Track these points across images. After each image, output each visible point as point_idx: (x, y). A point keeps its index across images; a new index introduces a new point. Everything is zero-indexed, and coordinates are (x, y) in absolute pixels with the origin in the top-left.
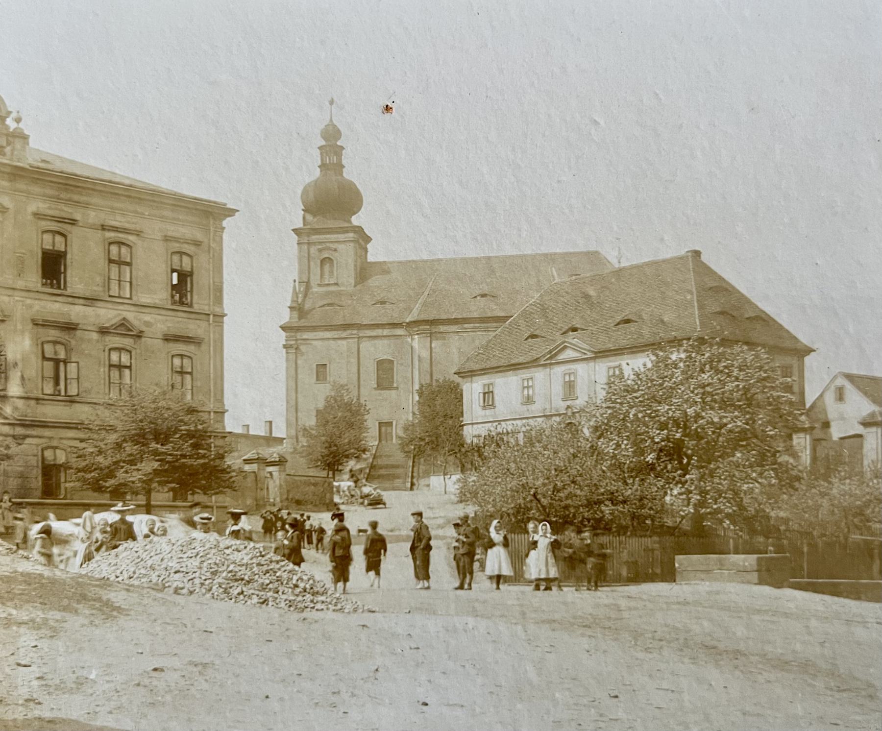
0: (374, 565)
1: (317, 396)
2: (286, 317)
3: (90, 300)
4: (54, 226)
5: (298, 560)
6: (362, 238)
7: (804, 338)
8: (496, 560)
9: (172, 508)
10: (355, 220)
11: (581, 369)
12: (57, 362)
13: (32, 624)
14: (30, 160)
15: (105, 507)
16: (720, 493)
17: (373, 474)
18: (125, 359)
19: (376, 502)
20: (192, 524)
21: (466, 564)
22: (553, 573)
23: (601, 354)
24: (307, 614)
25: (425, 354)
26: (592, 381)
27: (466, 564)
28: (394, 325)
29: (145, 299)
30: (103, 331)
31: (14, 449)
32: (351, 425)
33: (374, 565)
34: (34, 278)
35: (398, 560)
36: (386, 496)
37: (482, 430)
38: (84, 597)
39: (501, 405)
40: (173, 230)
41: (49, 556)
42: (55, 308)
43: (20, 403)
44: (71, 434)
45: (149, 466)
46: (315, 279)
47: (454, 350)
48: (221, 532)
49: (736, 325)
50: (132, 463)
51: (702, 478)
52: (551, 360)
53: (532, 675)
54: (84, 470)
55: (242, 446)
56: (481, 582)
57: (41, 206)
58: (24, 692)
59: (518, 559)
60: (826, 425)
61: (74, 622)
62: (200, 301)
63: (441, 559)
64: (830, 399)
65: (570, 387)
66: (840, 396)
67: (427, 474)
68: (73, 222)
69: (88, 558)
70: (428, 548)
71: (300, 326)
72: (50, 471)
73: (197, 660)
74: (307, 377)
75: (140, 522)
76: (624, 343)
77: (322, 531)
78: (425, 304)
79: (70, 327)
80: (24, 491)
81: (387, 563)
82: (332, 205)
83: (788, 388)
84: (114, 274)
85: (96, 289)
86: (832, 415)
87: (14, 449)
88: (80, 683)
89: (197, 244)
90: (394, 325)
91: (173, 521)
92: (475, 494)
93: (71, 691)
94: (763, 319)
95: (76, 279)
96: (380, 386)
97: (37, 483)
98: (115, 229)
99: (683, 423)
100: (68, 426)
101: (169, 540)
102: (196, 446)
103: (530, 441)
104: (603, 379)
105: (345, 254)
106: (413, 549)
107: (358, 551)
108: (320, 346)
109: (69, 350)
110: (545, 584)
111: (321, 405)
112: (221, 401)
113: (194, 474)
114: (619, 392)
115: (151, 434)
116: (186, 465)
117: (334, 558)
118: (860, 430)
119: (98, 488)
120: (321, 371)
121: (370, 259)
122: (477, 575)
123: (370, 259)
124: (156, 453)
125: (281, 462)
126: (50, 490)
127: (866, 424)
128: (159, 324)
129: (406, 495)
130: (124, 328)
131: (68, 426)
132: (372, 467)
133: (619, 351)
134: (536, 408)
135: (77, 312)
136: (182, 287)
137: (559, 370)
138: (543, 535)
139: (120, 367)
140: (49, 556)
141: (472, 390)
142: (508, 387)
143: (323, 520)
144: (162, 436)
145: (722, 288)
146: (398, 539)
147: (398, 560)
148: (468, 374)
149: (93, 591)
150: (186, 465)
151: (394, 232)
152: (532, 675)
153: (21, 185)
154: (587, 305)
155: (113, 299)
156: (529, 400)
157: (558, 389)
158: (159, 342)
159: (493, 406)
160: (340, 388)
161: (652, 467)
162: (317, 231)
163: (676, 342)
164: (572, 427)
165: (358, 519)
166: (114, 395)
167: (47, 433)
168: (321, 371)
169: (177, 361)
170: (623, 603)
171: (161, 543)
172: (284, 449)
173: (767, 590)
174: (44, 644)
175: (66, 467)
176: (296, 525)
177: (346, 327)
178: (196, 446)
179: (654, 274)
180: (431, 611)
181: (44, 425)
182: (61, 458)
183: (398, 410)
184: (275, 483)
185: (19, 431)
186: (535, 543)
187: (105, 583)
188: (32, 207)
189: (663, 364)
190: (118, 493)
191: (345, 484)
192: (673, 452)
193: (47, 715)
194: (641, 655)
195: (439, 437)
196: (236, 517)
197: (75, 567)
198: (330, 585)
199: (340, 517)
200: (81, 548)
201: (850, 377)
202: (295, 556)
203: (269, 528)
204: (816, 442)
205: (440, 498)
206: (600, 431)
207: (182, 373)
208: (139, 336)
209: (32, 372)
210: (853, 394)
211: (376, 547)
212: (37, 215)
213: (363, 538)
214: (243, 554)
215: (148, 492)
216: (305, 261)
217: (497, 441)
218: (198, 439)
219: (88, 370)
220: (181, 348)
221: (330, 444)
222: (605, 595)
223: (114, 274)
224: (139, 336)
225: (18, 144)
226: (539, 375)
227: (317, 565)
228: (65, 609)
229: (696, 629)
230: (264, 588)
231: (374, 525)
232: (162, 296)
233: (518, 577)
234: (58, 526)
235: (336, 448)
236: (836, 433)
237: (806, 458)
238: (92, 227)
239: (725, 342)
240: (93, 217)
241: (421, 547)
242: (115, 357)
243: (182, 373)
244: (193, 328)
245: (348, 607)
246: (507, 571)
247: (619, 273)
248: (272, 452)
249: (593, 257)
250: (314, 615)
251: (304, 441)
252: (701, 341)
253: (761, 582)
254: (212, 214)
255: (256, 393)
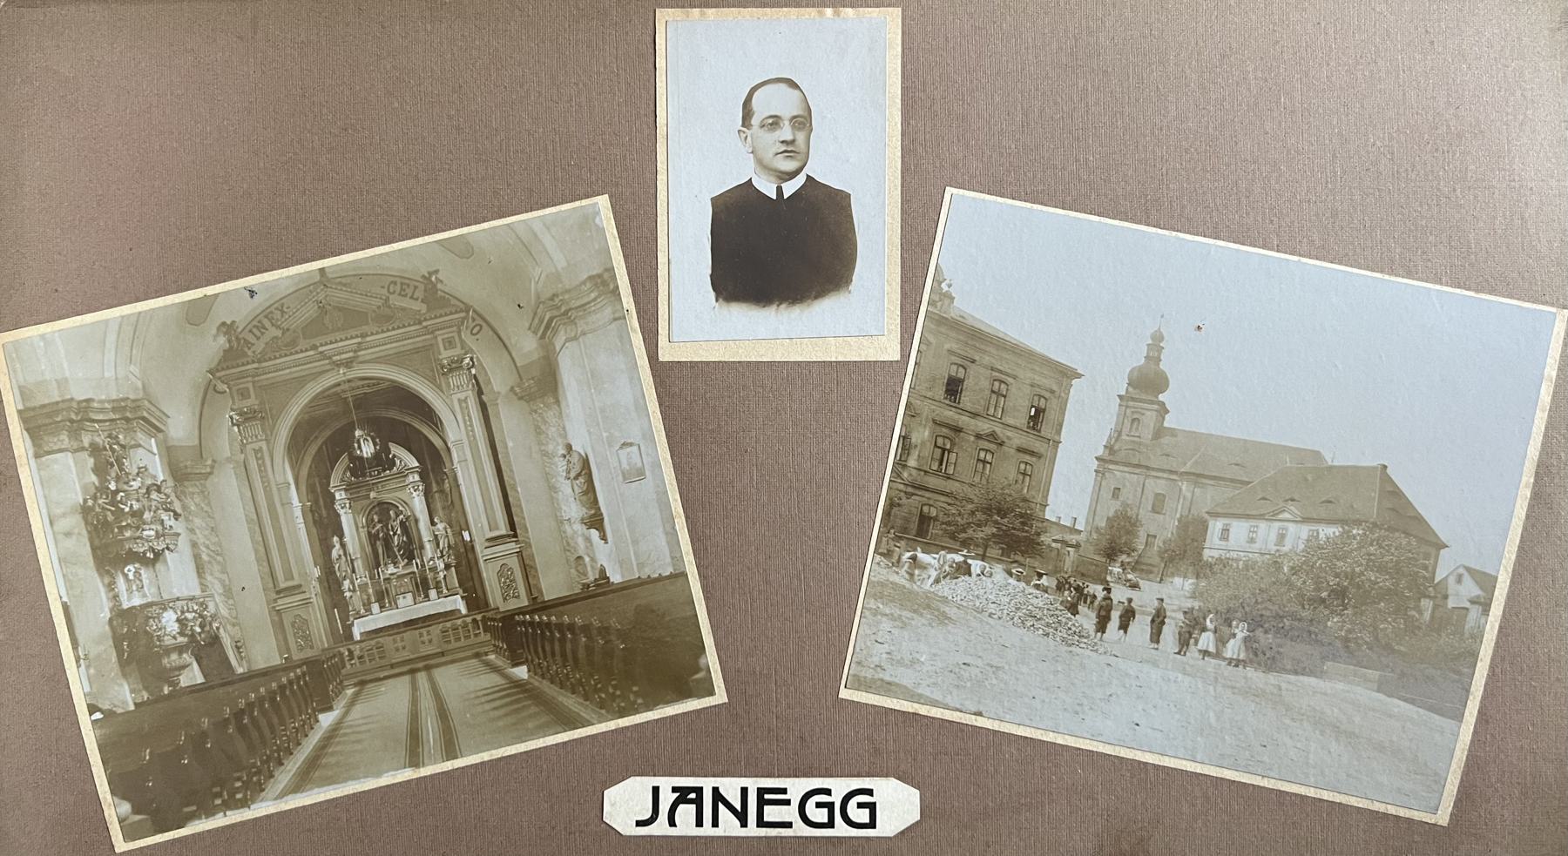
0: (1124, 627)
1: (1110, 508)
2: (1100, 451)
3: (975, 415)
4: (959, 361)
5: (1075, 612)
6: (1163, 410)
7: (1443, 537)
8: (1207, 640)
9: (999, 561)
10: (1161, 397)
11: (1292, 527)
12: (944, 450)
13: (892, 617)
14: (953, 314)
15: (956, 551)
16: (1364, 626)
17: (1136, 567)
18: (989, 458)
19: (1135, 586)
20: (1011, 574)
21: (1185, 640)
22: (1242, 657)
23: (1306, 520)
24: (1073, 648)
25: (1189, 495)
26: (1297, 535)
27: (1185, 640)
28: (1171, 472)
29: (1011, 421)
30: (978, 436)
31: (904, 501)
32: (1128, 532)
33: (1124, 627)
34: (940, 392)
35: (1141, 627)
36: (1141, 583)
37: (1216, 554)
38: (928, 606)
39: (1236, 540)
40: (1038, 379)
41: (912, 575)
42: (950, 414)
43: (914, 472)
44: (943, 498)
45: (990, 530)
46: (1125, 431)
47: (1207, 497)
48: (1028, 583)
49: (1399, 515)
50: (979, 526)
51: (1355, 614)
52: (1272, 517)
53: (1213, 720)
54: (948, 523)
55: (1054, 530)
56: (1193, 652)
57: (954, 346)
58: (876, 660)
59: (1222, 641)
60: (1446, 597)
61: (918, 621)
62: (1046, 430)
63: (1169, 633)
64: (1452, 580)
65: (1281, 537)
66: (1459, 580)
67: (1173, 575)
68: (973, 361)
69: (937, 581)
70: (1163, 623)
71: (1109, 459)
72: (924, 520)
73: (994, 663)
74: (1106, 494)
75: (976, 566)
76: (1324, 516)
77: (1095, 597)
78: (1196, 462)
79: (958, 430)
80: (905, 530)
81: (1133, 627)
82: (1147, 384)
83: (1425, 568)
84: (993, 402)
85: (980, 409)
86: (1450, 592)
87: (904, 501)
88: (914, 662)
89: (1052, 392)
90: (1171, 472)
91: (998, 569)
92: (1201, 594)
93: (906, 666)
94: (1419, 519)
95: (966, 400)
96: (1154, 511)
97: (914, 526)
98: (1000, 372)
99: (1351, 576)
100: (942, 493)
101: (994, 582)
102: (1023, 524)
103: (1247, 567)
104: (1304, 535)
105: (1149, 418)
106: (1153, 621)
107: (1115, 615)
108: (1119, 474)
109: (953, 444)
110: (1237, 663)
111: (1111, 514)
112: (1046, 497)
113: (1018, 541)
114: (1313, 545)
115: (995, 509)
116: (1014, 534)
117: (1098, 616)
118: (1468, 605)
119: (953, 537)
120: (1116, 492)
121: (1166, 424)
122: (1192, 647)
123: (1166, 424)
124: (996, 522)
125: (1077, 546)
126: (922, 531)
127: (1472, 602)
128: (1018, 439)
129: (1156, 586)
130: (992, 437)
131: (942, 493)
132: (1137, 562)
133: (1319, 521)
134: (1256, 546)
135: (964, 420)
136: (1037, 419)
137: (1277, 525)
138: (1241, 631)
139: (984, 462)
140: (912, 575)
141: (1216, 526)
142: (1239, 529)
143: (1097, 590)
144: (1002, 512)
145: (1397, 493)
146: (1143, 613)
147: (1141, 627)
148: (1215, 515)
149: (935, 604)
150: (1014, 534)
151: (1186, 410)
152: (1213, 720)
153: (943, 330)
154: (1303, 482)
155: (987, 417)
156: (1252, 541)
157: (1273, 537)
158: (1013, 451)
159: (1227, 539)
160: (1125, 505)
161: (1323, 601)
162: (1133, 399)
163: (1358, 523)
164: (1277, 565)
165: (1120, 594)
166: (977, 479)
167: (927, 494)
168: (1116, 492)
169: (1023, 466)
170: (1284, 686)
171: (986, 581)
172: (1082, 537)
173: (1381, 696)
174: (896, 632)
175: (936, 519)
176: (1079, 589)
177: (1138, 466)
178: (1023, 524)
179: (1352, 475)
180: (1155, 664)
181: (927, 489)
182: (934, 513)
183: (1160, 528)
184: (1069, 563)
185: (910, 490)
186: (1234, 635)
187: (945, 600)
188: (947, 346)
189: (1346, 535)
190: (965, 544)
191: (1117, 570)
192: (1340, 593)
193: (887, 678)
194: (1287, 721)
195: (1185, 552)
196: (1040, 576)
197: (927, 585)
198: (1092, 633)
199: (1108, 590)
200: (934, 574)
201: (1468, 569)
202: (1073, 608)
203: (1060, 587)
204: (1436, 607)
205: (1178, 592)
206: (1295, 571)
207: (1024, 474)
208: (1001, 444)
209: (927, 452)
210: (1467, 578)
211: (1128, 615)
212: (950, 352)
213: (1121, 607)
214: (1039, 600)
215: (986, 547)
216: (1122, 417)
217: (1224, 563)
218: (1026, 519)
219: (963, 461)
220: (1027, 458)
221: (1112, 541)
222: (1272, 678)
223: (993, 402)
224: (1001, 444)
225: (947, 302)
226: (1263, 525)
227: (1086, 619)
228: (915, 611)
229: (1328, 712)
230: (1048, 625)
231: (1130, 600)
232: (1021, 420)
233: (1218, 655)
234: (920, 555)
235: (1116, 543)
236: (1451, 604)
237: (1427, 616)
238: (985, 367)
239: (1391, 529)
240: (987, 360)
241: (1158, 620)
242: (982, 455)
243: (1024, 474)
244: (1038, 446)
245: (1101, 650)
246: (1212, 649)
247: (1331, 467)
248: (1073, 539)
249: (1317, 455)
250: (1078, 650)
251: (1095, 536)
252: (1375, 525)
253: (1378, 691)
254: (1067, 374)
255: (1070, 499)
